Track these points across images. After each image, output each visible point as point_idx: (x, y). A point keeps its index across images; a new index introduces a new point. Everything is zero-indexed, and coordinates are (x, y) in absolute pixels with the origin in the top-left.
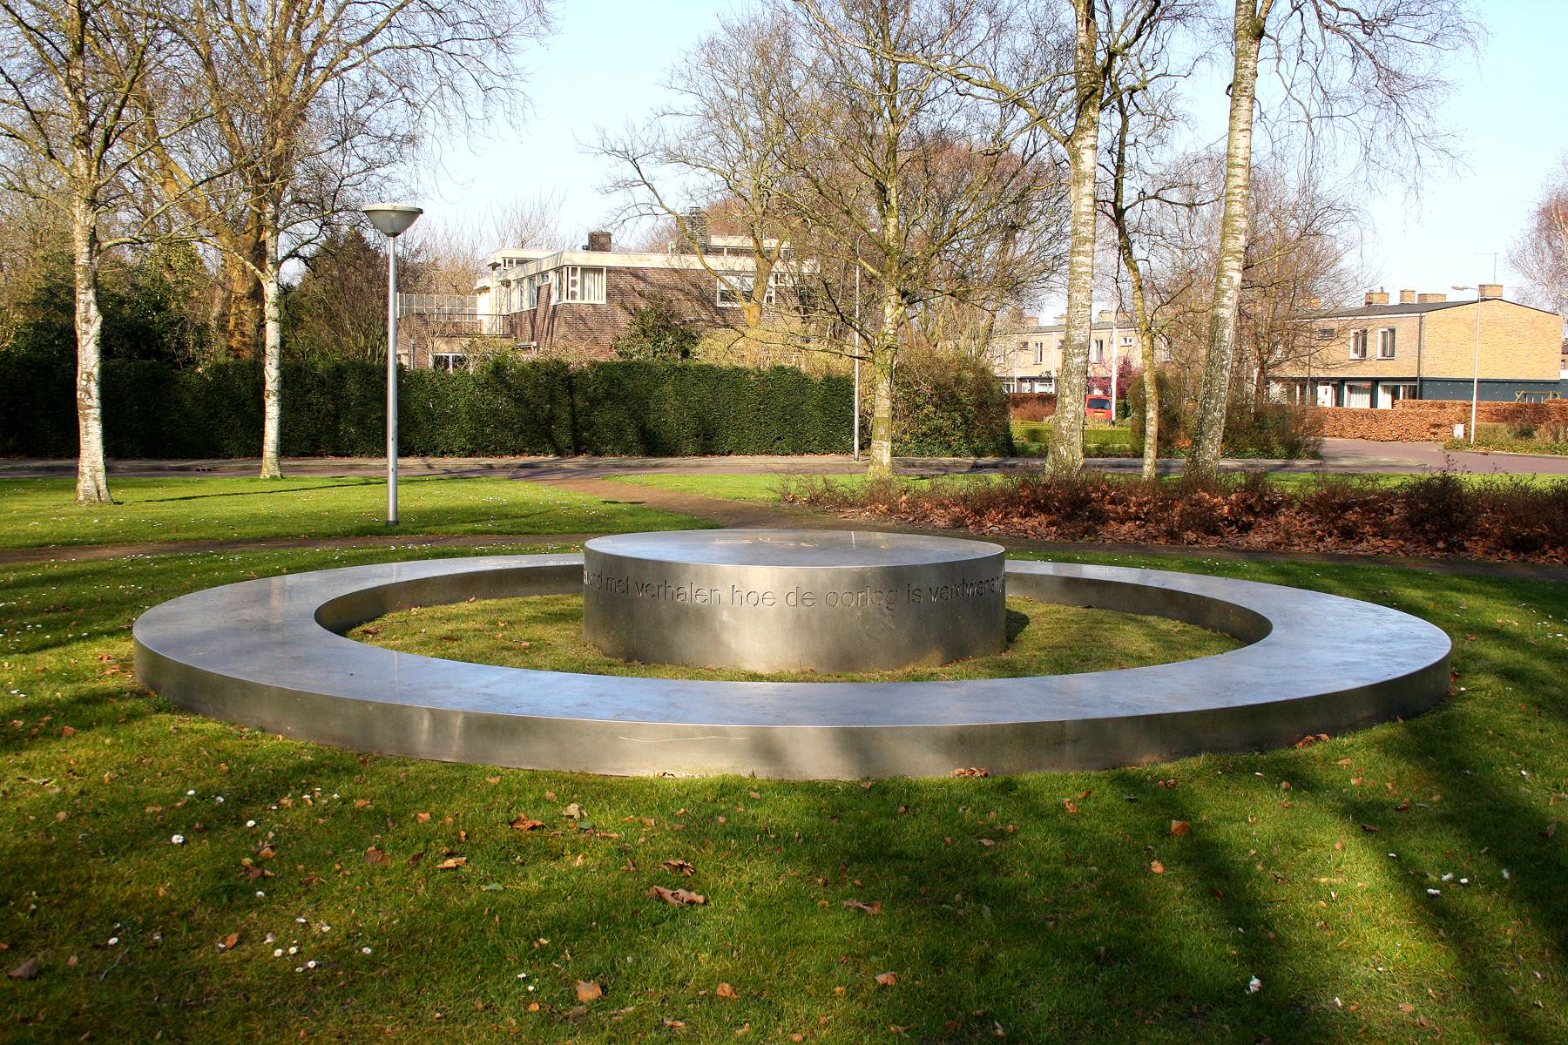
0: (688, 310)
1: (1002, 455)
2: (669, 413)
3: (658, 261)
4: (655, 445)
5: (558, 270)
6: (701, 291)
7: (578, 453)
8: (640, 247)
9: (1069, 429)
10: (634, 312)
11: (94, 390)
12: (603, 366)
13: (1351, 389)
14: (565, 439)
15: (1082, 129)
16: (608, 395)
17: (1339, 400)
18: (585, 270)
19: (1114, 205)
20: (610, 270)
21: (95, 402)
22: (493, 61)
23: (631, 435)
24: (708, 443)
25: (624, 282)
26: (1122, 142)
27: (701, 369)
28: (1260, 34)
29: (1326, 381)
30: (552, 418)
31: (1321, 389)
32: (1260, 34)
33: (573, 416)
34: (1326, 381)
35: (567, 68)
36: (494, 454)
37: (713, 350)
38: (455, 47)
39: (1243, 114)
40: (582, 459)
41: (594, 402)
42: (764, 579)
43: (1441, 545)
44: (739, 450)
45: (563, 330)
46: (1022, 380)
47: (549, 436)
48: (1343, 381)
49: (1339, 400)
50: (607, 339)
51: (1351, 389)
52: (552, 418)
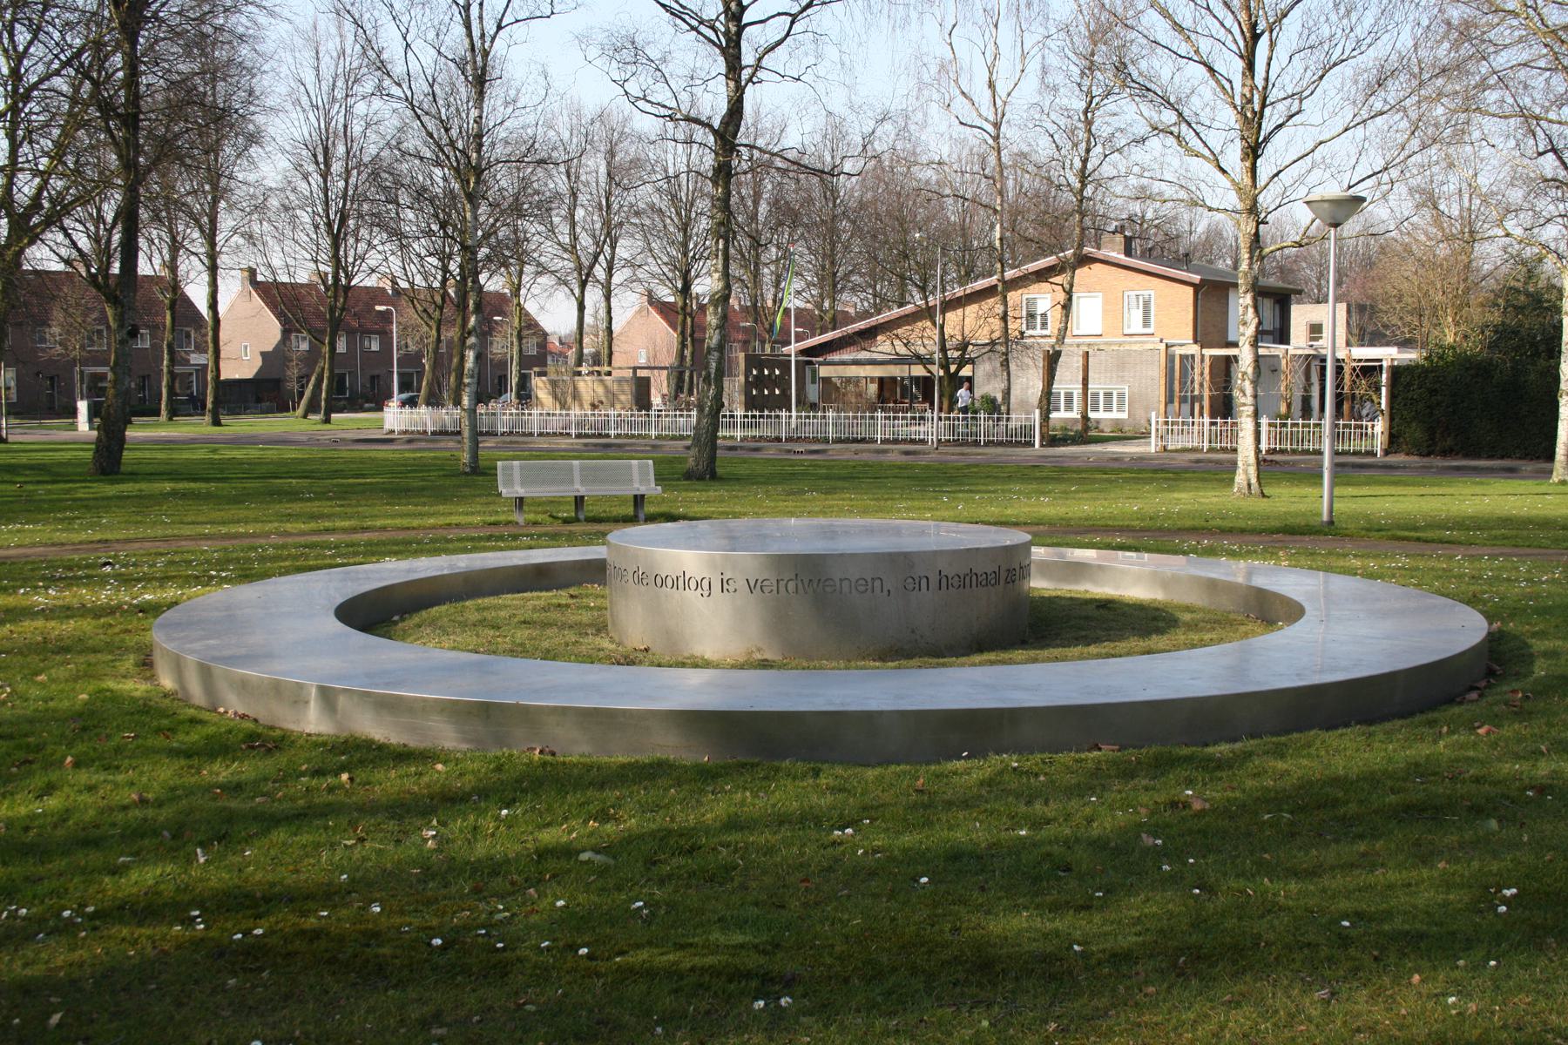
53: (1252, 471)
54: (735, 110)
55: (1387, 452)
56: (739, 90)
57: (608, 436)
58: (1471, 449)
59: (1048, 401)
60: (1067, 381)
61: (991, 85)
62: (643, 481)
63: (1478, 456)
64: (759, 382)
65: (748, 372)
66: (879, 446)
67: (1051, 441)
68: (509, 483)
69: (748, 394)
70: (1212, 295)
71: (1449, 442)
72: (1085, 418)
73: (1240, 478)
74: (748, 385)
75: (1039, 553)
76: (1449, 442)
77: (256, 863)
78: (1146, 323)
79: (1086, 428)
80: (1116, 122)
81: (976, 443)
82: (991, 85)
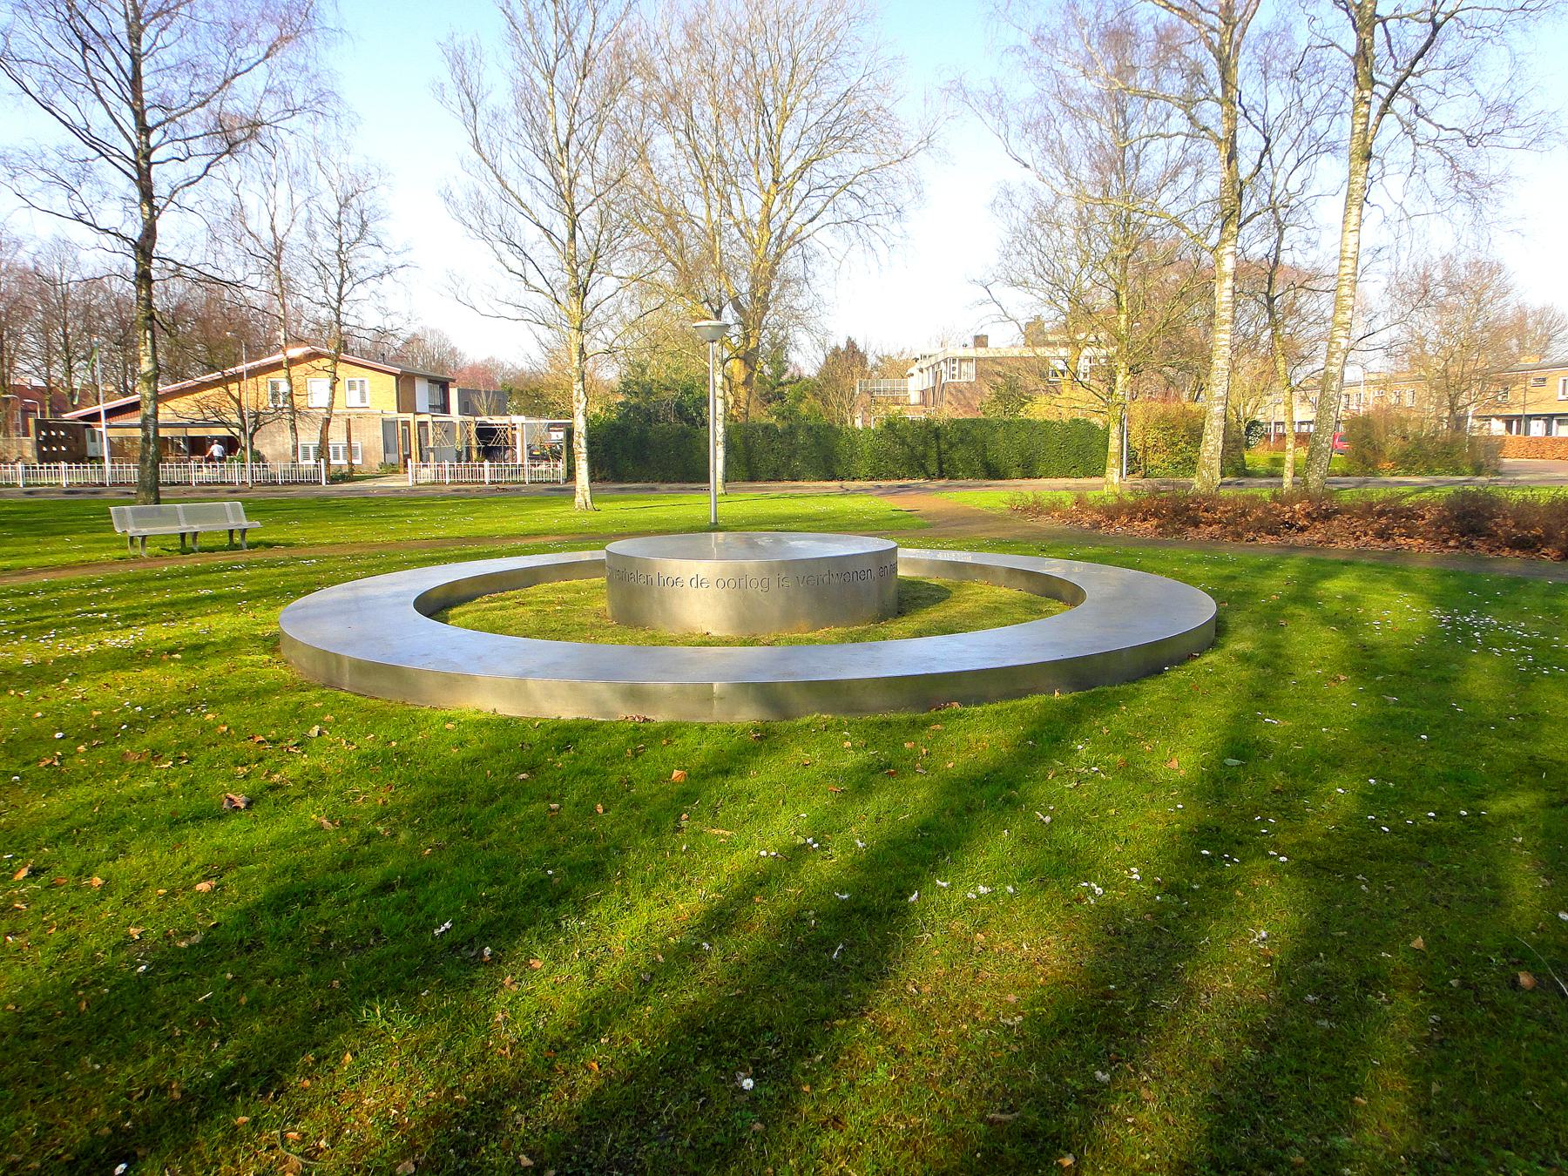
0: (1030, 381)
1: (1238, 475)
2: (1001, 450)
3: (1016, 352)
4: (993, 472)
5: (945, 361)
6: (1041, 371)
7: (941, 477)
8: (1005, 341)
9: (1210, 458)
10: (995, 387)
11: (583, 443)
12: (958, 421)
13: (1559, 422)
14: (933, 468)
15: (1224, 241)
16: (961, 441)
17: (1549, 431)
18: (961, 360)
19: (1267, 294)
20: (978, 359)
21: (584, 450)
22: (895, 228)
23: (978, 465)
24: (1029, 470)
25: (988, 366)
26: (1278, 247)
27: (1022, 422)
28: (1368, 156)
29: (1537, 417)
30: (924, 456)
31: (1533, 423)
32: (1368, 156)
33: (939, 454)
34: (1537, 417)
35: (418, 221)
36: (886, 478)
37: (1040, 410)
38: (871, 220)
39: (1353, 219)
40: (942, 482)
41: (952, 446)
42: (704, 568)
43: (1452, 543)
44: (1046, 475)
45: (947, 397)
46: (1302, 423)
47: (922, 466)
48: (1552, 416)
49: (1549, 431)
50: (977, 404)
51: (1559, 422)
52: (924, 456)
53: (587, 494)
54: (150, 232)
55: (566, 481)
56: (153, 214)
57: (15, 485)
58: (619, 477)
59: (322, 450)
60: (337, 438)
61: (273, 229)
62: (237, 518)
63: (621, 481)
64: (48, 441)
65: (38, 434)
66: (487, 486)
67: (333, 480)
68: (123, 523)
69: (39, 450)
70: (405, 381)
71: (604, 473)
72: (351, 464)
73: (579, 499)
74: (39, 444)
75: (903, 553)
76: (604, 473)
77: (790, 894)
78: (363, 399)
79: (352, 471)
80: (363, 262)
81: (275, 483)
82: (273, 229)
